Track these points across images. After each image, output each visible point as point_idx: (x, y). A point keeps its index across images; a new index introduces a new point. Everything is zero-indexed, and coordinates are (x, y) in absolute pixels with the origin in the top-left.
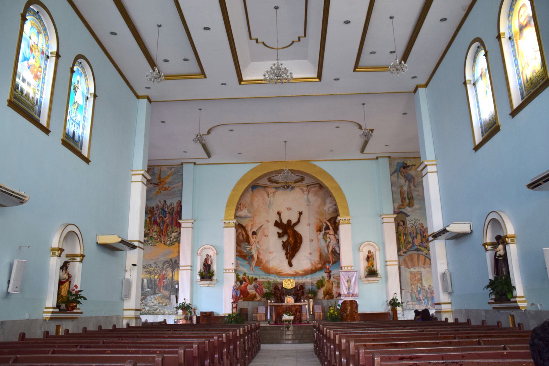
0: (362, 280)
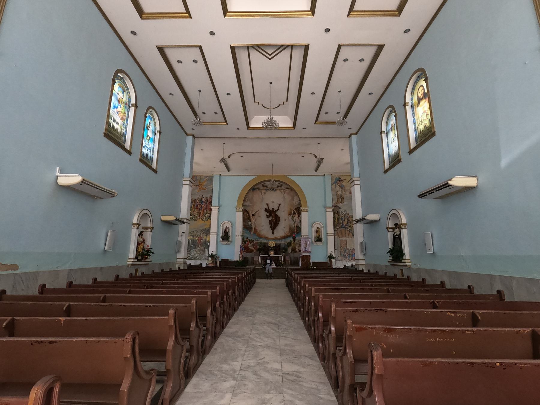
0: (313, 243)
